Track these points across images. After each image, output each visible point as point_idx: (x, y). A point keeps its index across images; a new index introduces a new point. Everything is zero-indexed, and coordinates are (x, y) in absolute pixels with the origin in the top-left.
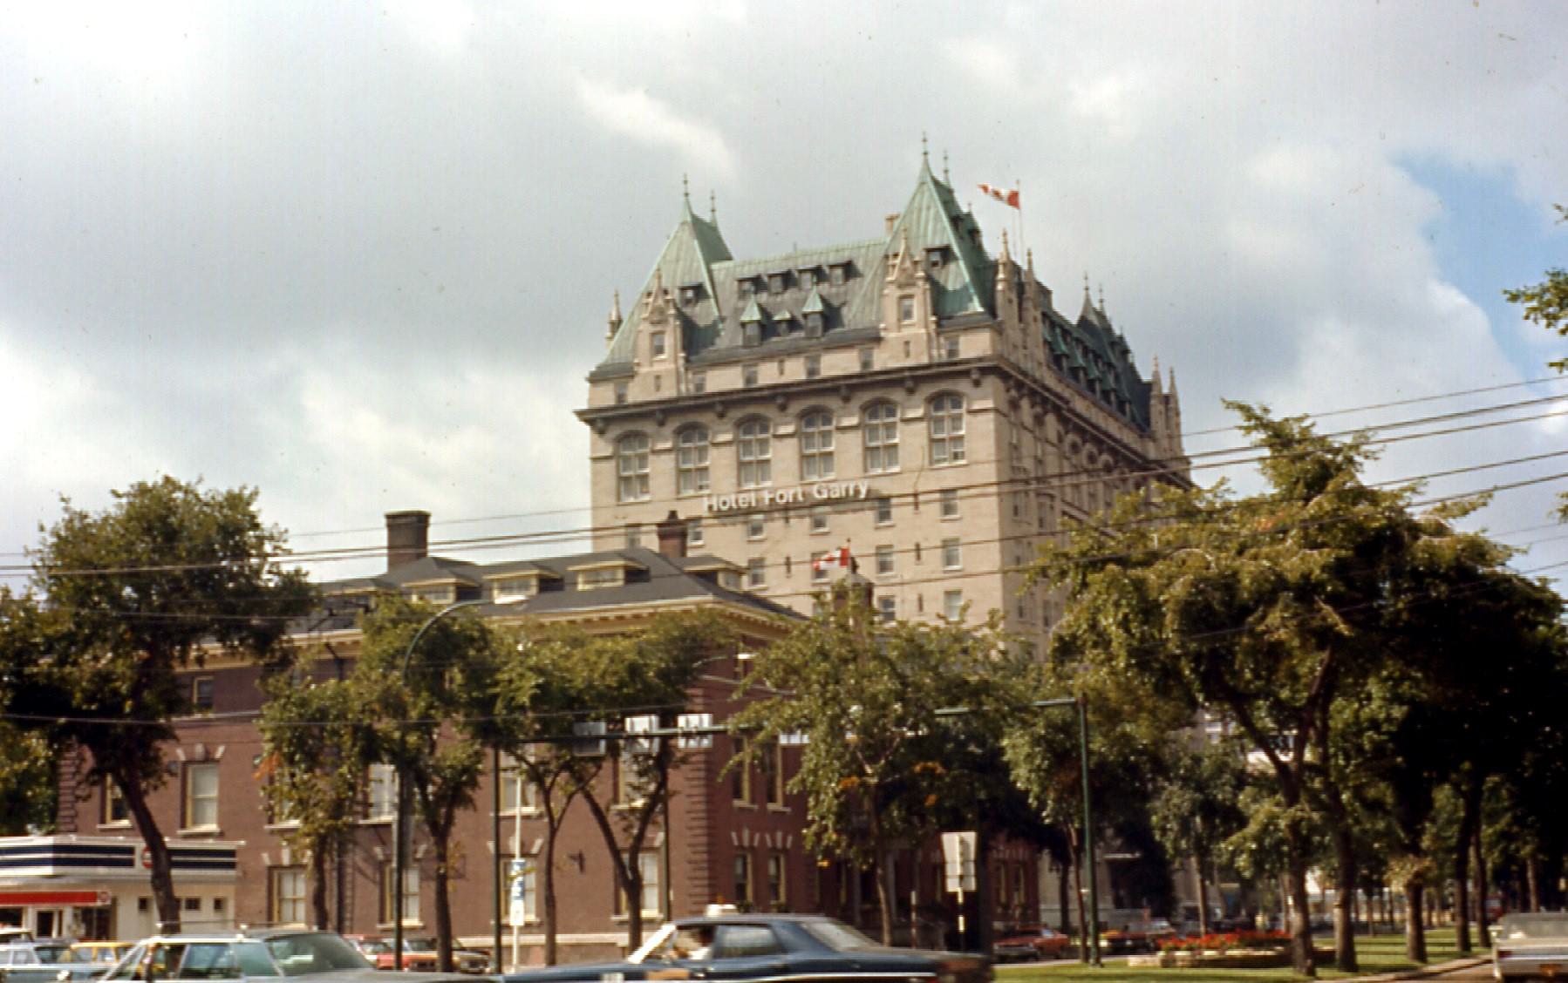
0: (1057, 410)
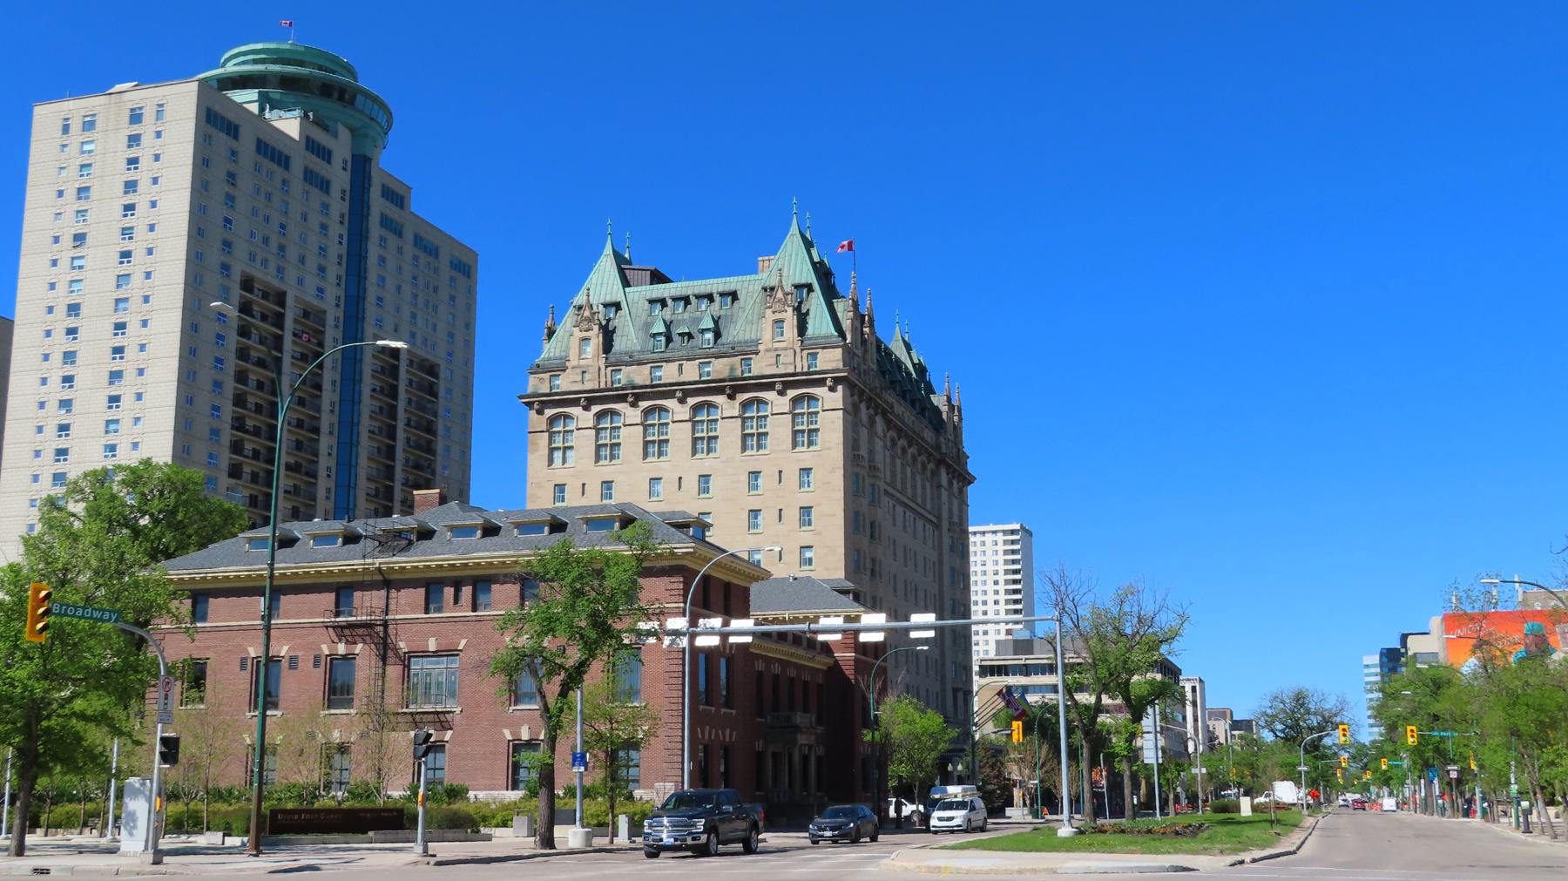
0: (884, 413)
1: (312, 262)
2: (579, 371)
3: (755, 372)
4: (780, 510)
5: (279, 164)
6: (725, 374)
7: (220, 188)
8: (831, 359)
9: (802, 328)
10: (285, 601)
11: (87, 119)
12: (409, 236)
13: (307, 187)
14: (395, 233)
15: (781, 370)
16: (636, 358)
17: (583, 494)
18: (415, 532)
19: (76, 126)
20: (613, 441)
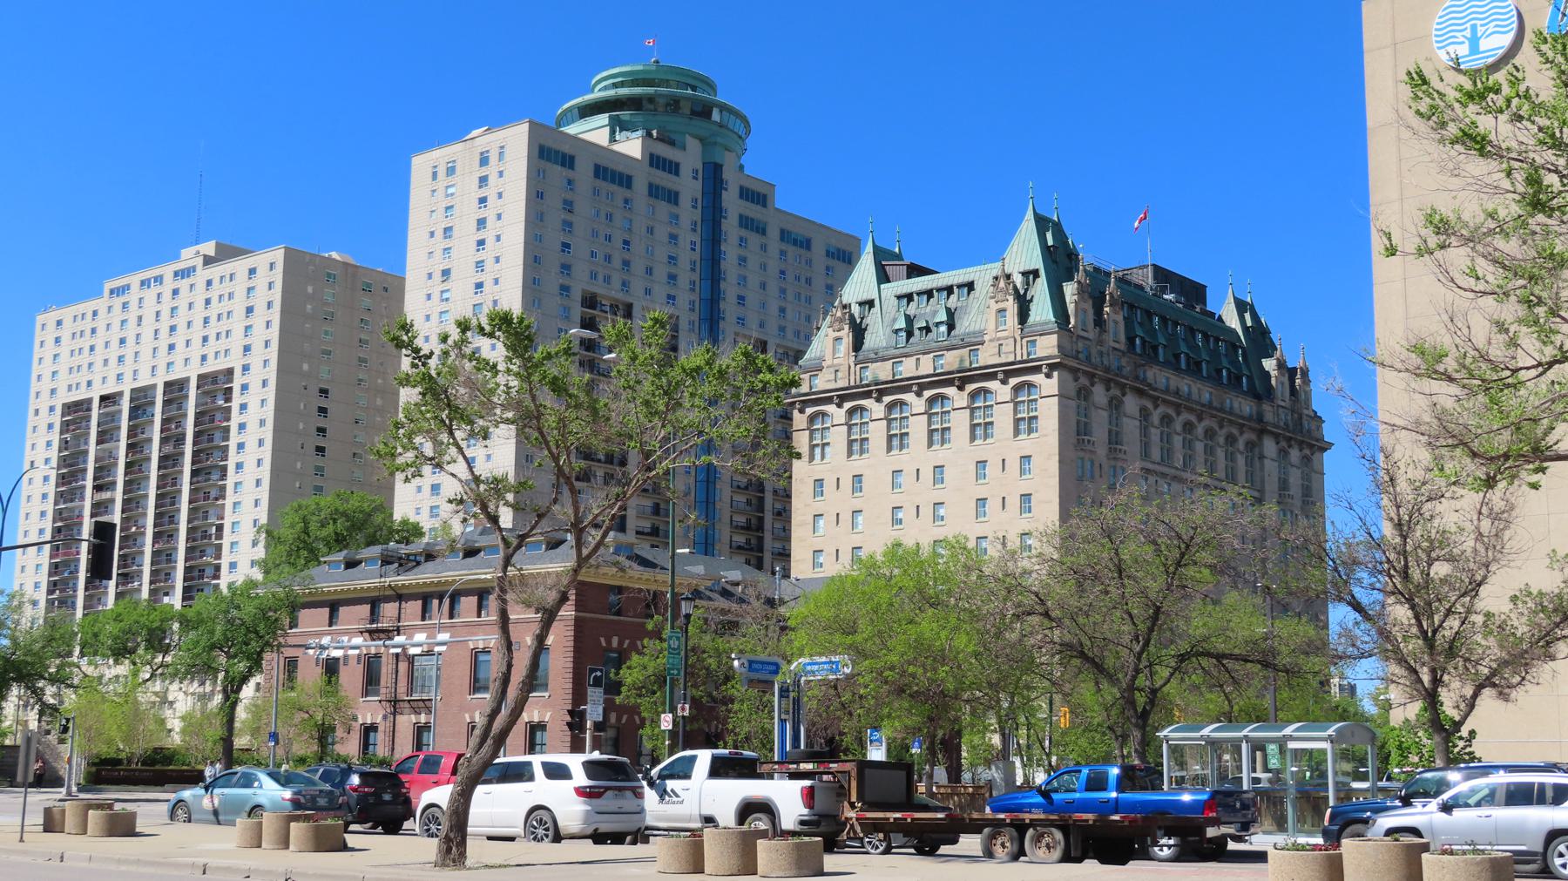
1: (661, 272)
2: (832, 370)
3: (981, 363)
4: (1004, 498)
5: (621, 184)
6: (955, 367)
7: (556, 216)
8: (1048, 346)
9: (1023, 315)
10: (343, 610)
11: (450, 165)
12: (773, 233)
13: (652, 201)
14: (758, 232)
15: (1003, 360)
16: (880, 355)
17: (838, 488)
18: (424, 554)
19: (442, 171)
20: (1031, 414)
